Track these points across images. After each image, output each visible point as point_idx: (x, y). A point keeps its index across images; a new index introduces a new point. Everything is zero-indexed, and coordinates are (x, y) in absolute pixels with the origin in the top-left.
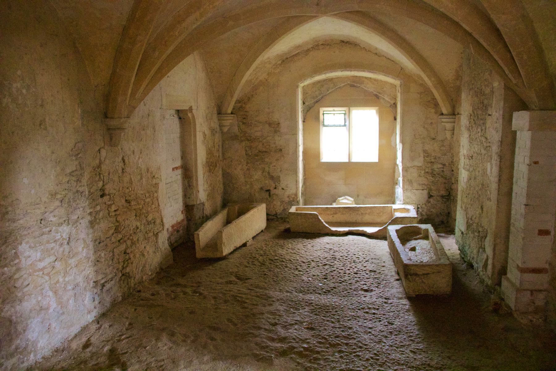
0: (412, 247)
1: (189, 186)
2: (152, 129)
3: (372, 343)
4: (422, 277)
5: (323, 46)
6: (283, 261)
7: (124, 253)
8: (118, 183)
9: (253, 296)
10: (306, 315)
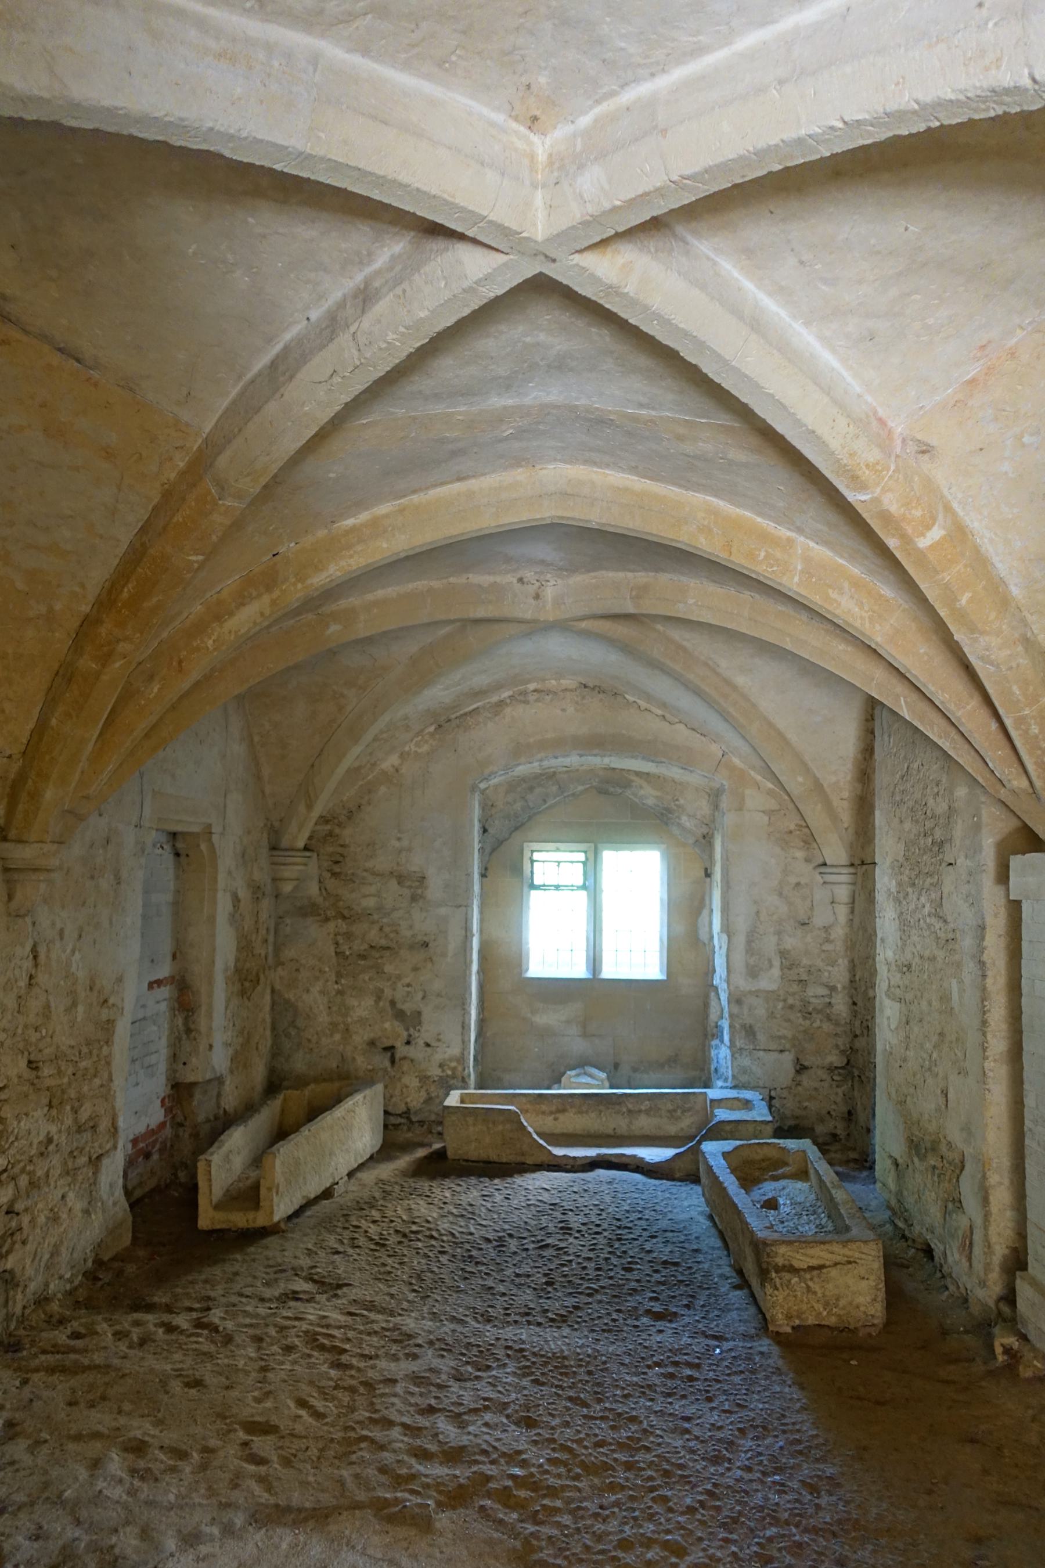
0: (766, 1198)
1: (188, 1031)
2: (112, 877)
3: (696, 1460)
4: (808, 1276)
5: (536, 695)
6: (432, 1237)
7: (7, 1213)
8: (16, 1014)
9: (361, 1332)
10: (510, 1385)
